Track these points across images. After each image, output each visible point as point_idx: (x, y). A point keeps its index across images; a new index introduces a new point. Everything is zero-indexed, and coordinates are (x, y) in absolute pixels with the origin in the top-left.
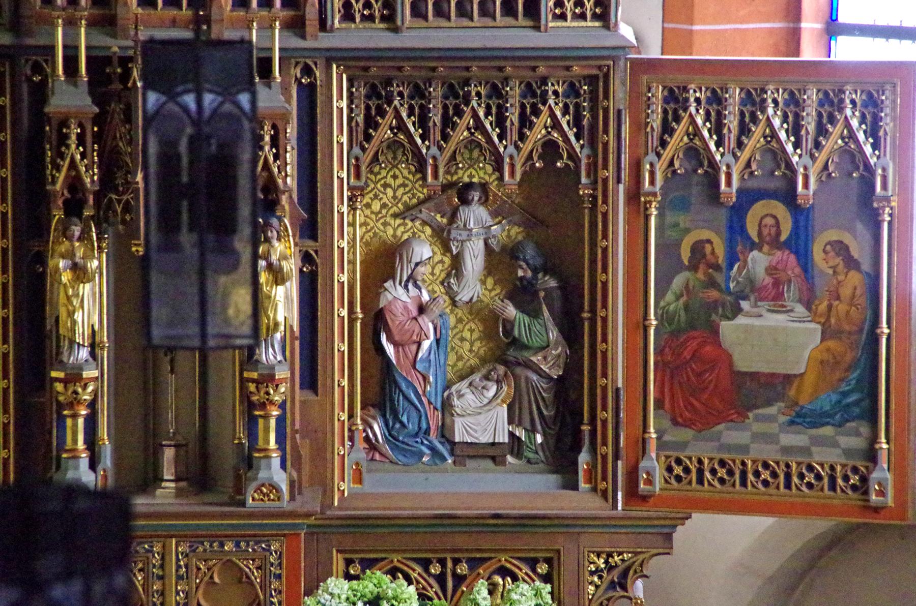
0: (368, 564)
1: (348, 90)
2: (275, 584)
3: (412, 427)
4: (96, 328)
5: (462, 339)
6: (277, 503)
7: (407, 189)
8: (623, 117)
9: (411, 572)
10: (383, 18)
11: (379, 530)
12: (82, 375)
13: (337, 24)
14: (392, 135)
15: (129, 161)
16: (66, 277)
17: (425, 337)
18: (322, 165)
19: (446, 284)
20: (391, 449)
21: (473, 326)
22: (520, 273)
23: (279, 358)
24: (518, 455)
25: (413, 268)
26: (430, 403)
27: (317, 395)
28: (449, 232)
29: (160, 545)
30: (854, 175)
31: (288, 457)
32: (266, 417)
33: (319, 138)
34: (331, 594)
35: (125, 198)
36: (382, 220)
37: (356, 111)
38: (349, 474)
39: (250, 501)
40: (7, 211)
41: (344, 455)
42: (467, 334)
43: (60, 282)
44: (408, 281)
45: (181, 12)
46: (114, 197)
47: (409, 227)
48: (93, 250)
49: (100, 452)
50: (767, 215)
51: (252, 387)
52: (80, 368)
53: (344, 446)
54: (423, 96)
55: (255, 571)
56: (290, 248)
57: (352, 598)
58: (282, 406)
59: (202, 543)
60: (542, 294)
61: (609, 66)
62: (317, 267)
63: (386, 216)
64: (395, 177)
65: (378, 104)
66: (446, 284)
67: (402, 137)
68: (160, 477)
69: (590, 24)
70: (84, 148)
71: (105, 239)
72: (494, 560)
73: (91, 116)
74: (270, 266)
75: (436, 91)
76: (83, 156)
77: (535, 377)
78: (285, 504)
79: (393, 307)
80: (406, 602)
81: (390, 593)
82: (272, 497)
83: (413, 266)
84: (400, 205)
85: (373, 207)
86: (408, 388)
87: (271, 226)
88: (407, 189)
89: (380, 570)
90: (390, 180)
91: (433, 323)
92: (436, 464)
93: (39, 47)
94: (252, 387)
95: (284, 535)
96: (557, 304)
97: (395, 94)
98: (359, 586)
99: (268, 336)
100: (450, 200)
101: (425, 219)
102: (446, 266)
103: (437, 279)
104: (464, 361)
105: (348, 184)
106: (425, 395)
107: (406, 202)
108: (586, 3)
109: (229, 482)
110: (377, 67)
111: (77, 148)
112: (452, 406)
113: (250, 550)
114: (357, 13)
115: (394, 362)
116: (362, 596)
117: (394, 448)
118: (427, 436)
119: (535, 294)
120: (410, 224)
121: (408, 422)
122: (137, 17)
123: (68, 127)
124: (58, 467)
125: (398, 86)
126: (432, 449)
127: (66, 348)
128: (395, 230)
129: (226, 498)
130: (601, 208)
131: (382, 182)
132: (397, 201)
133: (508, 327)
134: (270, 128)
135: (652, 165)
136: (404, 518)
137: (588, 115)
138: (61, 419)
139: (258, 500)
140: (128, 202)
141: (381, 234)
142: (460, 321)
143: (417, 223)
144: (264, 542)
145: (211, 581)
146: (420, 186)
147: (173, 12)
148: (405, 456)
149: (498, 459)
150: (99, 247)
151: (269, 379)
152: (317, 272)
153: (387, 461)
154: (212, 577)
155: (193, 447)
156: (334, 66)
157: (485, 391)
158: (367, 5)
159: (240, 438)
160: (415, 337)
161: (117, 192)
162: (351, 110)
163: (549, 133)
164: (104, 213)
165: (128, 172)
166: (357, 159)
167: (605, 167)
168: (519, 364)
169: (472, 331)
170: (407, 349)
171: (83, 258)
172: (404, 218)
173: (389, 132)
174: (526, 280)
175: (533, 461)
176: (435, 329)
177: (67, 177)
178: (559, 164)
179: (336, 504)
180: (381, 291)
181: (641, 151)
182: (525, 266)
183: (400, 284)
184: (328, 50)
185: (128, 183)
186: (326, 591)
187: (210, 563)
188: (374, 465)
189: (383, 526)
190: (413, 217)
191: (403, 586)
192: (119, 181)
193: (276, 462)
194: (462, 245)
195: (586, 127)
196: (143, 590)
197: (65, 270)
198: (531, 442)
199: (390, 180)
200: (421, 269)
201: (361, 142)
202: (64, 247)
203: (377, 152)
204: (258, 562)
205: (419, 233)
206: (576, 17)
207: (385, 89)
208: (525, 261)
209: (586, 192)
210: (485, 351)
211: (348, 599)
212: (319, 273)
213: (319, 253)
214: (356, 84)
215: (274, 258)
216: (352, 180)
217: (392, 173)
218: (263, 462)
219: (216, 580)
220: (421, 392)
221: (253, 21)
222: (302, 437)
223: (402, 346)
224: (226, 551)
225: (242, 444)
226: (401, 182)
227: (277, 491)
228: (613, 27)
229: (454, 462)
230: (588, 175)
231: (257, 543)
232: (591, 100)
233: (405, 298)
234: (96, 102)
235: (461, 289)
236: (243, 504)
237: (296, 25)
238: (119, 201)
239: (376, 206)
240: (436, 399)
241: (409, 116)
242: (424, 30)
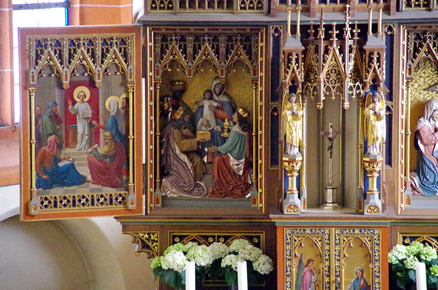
0: (413, 239)
1: (407, 36)
2: (377, 248)
3: (432, 180)
4: (301, 140)
6: (377, 213)
7: (430, 78)
9: (432, 242)
10: (424, 5)
11: (416, 225)
12: (296, 159)
13: (404, 9)
14: (425, 55)
15: (317, 70)
16: (290, 118)
18: (395, 68)
20: (422, 189)
23: (379, 152)
27: (392, 167)
29: (328, 230)
30: (52, 76)
31: (381, 194)
32: (372, 177)
34: (398, 252)
35: (314, 85)
36: (419, 92)
37: (410, 46)
38: (404, 200)
39: (366, 213)
40: (262, 90)
41: (402, 192)
43: (287, 120)
44: (430, 118)
45: (337, 5)
46: (309, 84)
47: (430, 94)
48: (300, 106)
49: (302, 190)
50: (80, 92)
51: (367, 164)
52: (295, 156)
53: (402, 189)
54: (93, 45)
55: (368, 242)
56: (383, 105)
57: (408, 254)
58: (379, 172)
59: (346, 230)
63: (420, 90)
64: (425, 73)
65: (420, 42)
67: (430, 56)
68: (326, 201)
70: (298, 64)
71: (305, 102)
72: (421, 237)
73: (302, 51)
74: (375, 113)
75: (222, 38)
76: (298, 67)
78: (381, 214)
80: (432, 256)
81: (425, 252)
82: (375, 211)
83: (433, 111)
84: (426, 85)
87: (376, 96)
88: (430, 78)
89: (418, 241)
90: (422, 74)
93: (278, 22)
94: (367, 164)
95: (380, 227)
97: (428, 38)
98: (410, 248)
99: (374, 142)
105: (406, 77)
107: (429, 84)
108: (157, 1)
109: (354, 203)
110: (420, 26)
111: (296, 64)
113: (366, 233)
114: (413, 3)
115: (424, 153)
116: (412, 253)
117: (424, 189)
120: (431, 93)
121: (430, 178)
122: (322, 9)
123: (292, 56)
124: (285, 197)
125: (429, 34)
127: (289, 148)
128: (424, 96)
129: (354, 211)
131: (419, 75)
132: (425, 83)
134: (376, 54)
135: (33, 73)
136: (430, 220)
138: (286, 177)
139: (369, 212)
140: (315, 86)
141: (418, 97)
143: (434, 93)
144: (372, 230)
145: (350, 246)
146: (436, 77)
147: (334, 5)
150: (303, 106)
151: (374, 161)
152: (392, 115)
153: (420, 194)
154: (350, 244)
155: (340, 189)
156: (402, 26)
158: (251, 2)
159: (361, 186)
160: (433, 142)
161: (311, 83)
162: (408, 45)
164: (305, 91)
165: (316, 74)
166: (410, 66)
170: (429, 147)
171: (296, 110)
172: (428, 91)
173: (424, 54)
177: (291, 76)
179: (399, 213)
180: (418, 122)
181: (28, 67)
183: (427, 119)
184: (398, 20)
185: (316, 78)
186: (396, 250)
187: (349, 238)
188: (415, 196)
189: (417, 223)
191: (430, 248)
192: (312, 78)
193: (377, 196)
196: (321, 249)
197: (289, 115)
199: (422, 74)
201: (412, 59)
202: (289, 105)
203: (419, 63)
204: (369, 238)
205: (435, 97)
207: (423, 36)
211: (406, 254)
213: (393, 107)
214: (410, 34)
215: (377, 110)
216: (407, 75)
217: (423, 71)
218: (371, 196)
219: (352, 245)
220: (435, 166)
221: (371, 9)
222: (386, 185)
223: (427, 146)
224: (356, 233)
225: (362, 188)
226: (428, 75)
227: (377, 209)
231: (369, 230)
234: (303, 45)
236: (363, 213)
237: (387, 10)
238: (312, 86)
241: (433, 47)
242: (215, 13)
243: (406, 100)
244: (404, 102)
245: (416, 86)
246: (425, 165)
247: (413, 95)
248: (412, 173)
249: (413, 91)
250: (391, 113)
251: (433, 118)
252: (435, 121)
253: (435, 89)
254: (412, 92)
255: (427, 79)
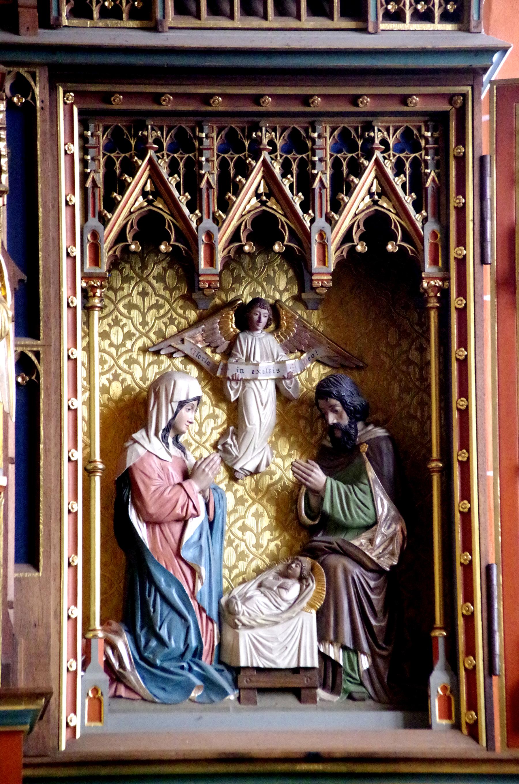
5: (244, 528)
7: (162, 312)
8: (488, 165)
14: (146, 204)
17: (194, 512)
19: (219, 447)
20: (143, 678)
21: (261, 510)
22: (332, 419)
24: (334, 689)
25: (175, 410)
26: (202, 609)
28: (225, 368)
33: (40, 186)
36: (126, 357)
42: (250, 521)
44: (167, 430)
54: (190, 148)
60: (365, 448)
61: (464, 96)
62: (38, 377)
63: (131, 350)
64: (144, 294)
66: (219, 447)
69: (438, 26)
77: (356, 571)
79: (145, 465)
83: (175, 406)
84: (151, 335)
85: (113, 338)
86: (169, 586)
88: (162, 312)
91: (204, 496)
92: (212, 702)
96: (388, 462)
100: (223, 326)
101: (188, 352)
102: (220, 421)
103: (206, 441)
104: (248, 560)
106: (194, 598)
107: (160, 330)
112: (233, 613)
118: (196, 660)
119: (357, 448)
121: (170, 638)
126: (206, 679)
130: (455, 302)
131: (126, 301)
133: (313, 501)
137: (433, 174)
142: (240, 501)
148: (164, 689)
149: (304, 693)
153: (137, 697)
156: (61, 90)
157: (283, 592)
160: (178, 510)
163: (375, 203)
167: (462, 242)
168: (334, 551)
169: (257, 516)
173: (141, 199)
174: (341, 429)
175: (356, 695)
176: (207, 505)
178: (390, 247)
180: (127, 444)
182: (339, 408)
183: (156, 434)
190: (172, 350)
194: (244, 387)
195: (430, 191)
198: (353, 670)
199: (137, 300)
200: (186, 414)
206: (418, 16)
207: (136, 135)
208: (340, 399)
209: (432, 283)
210: (277, 545)
212: (42, 386)
228: (476, 27)
229: (239, 699)
230: (435, 262)
232: (437, 152)
233: (163, 454)
235: (242, 453)
239: (117, 335)
240: (210, 603)
243: (85, 383)
244: (77, 404)
245: (117, 335)
246: (153, 589)
247: (106, 367)
248: (109, 624)
249: (109, 354)
250: (33, 378)
251: (176, 439)
252: (182, 449)
253: (179, 346)
254: (105, 356)
255: (154, 313)
